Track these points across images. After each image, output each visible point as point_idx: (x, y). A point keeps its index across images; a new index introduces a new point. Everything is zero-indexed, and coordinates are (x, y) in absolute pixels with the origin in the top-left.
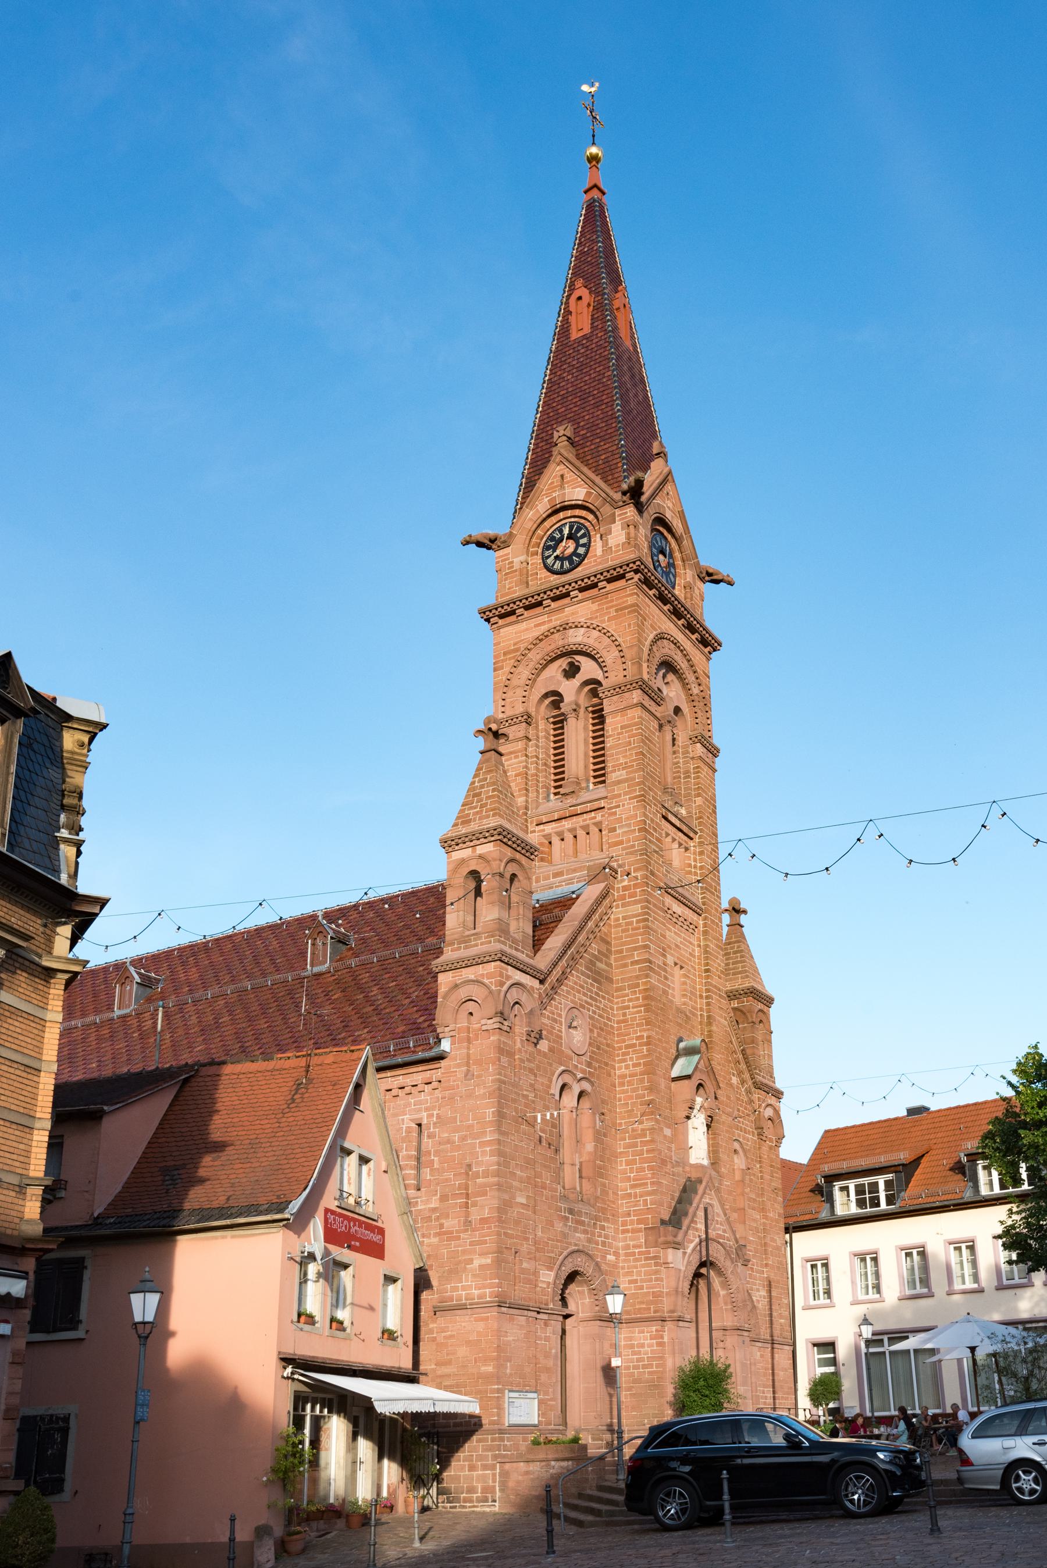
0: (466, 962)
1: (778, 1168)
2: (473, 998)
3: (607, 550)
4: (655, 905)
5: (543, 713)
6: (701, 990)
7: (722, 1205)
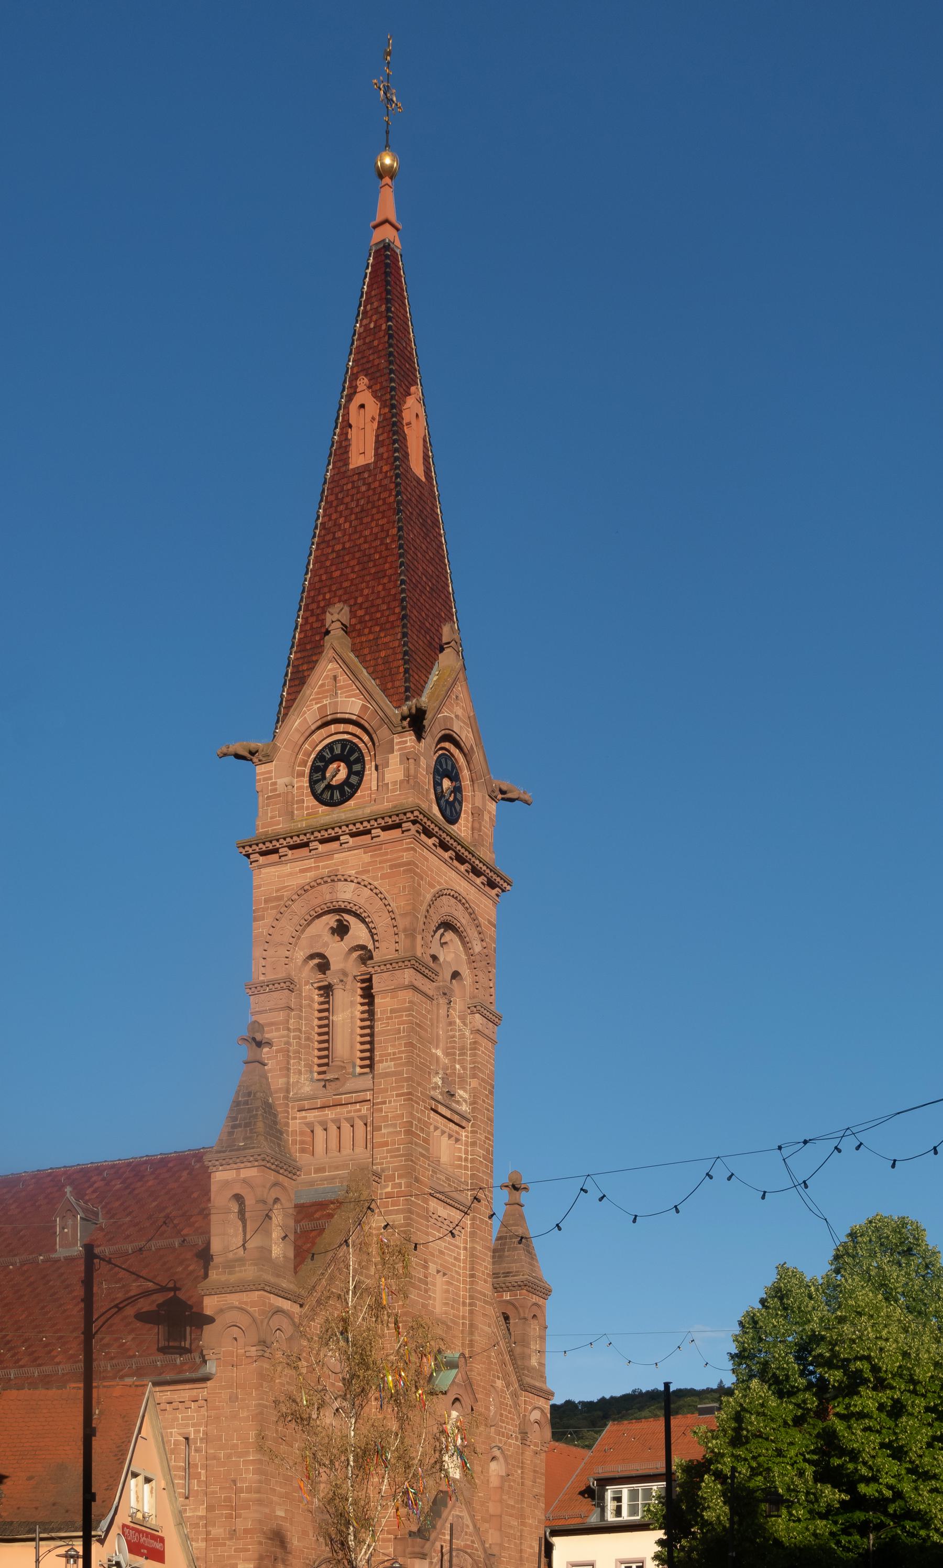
0: (231, 1288)
1: (542, 1474)
2: (238, 1324)
3: (382, 785)
4: (418, 1215)
5: (308, 979)
6: (464, 1297)
7: (472, 1517)
